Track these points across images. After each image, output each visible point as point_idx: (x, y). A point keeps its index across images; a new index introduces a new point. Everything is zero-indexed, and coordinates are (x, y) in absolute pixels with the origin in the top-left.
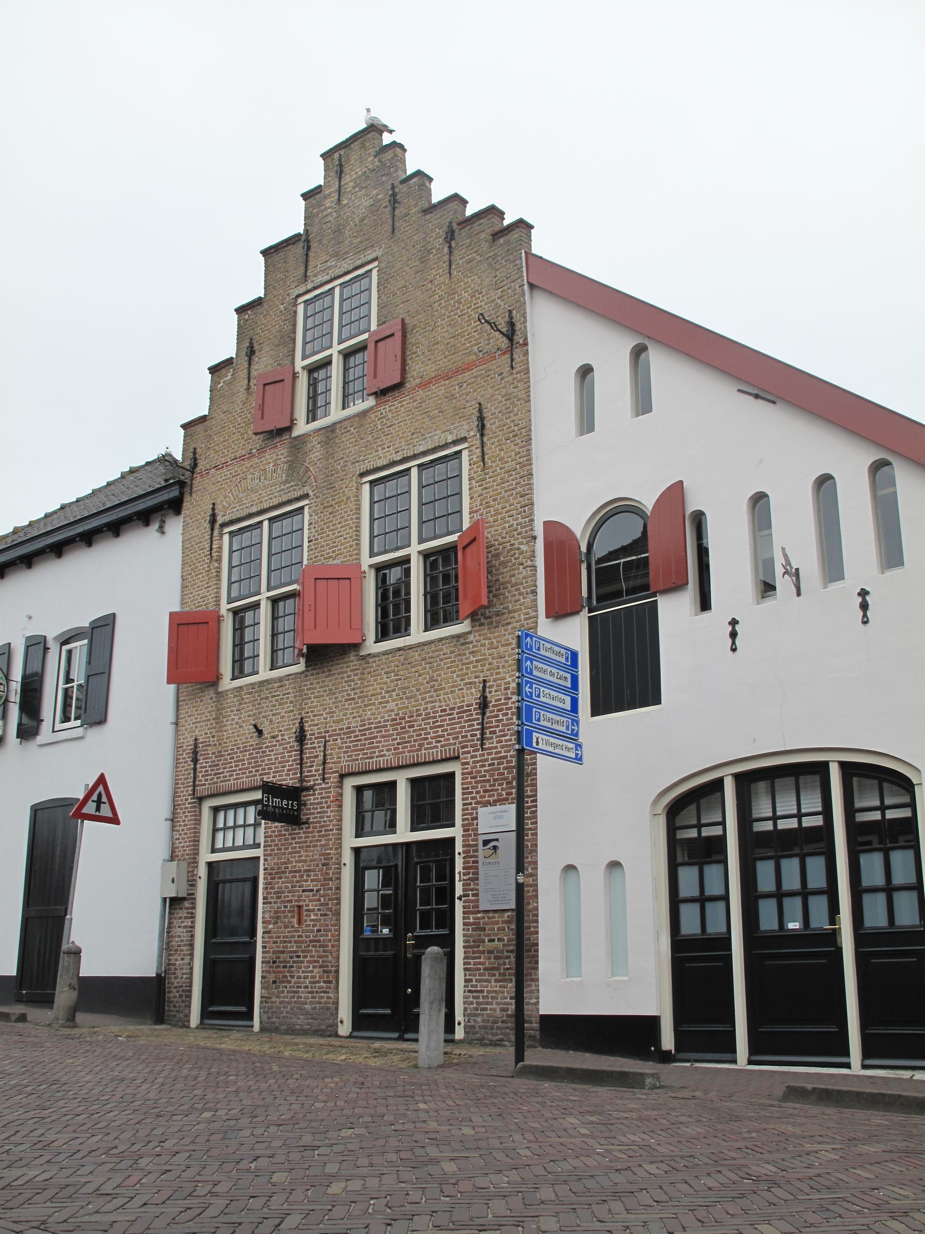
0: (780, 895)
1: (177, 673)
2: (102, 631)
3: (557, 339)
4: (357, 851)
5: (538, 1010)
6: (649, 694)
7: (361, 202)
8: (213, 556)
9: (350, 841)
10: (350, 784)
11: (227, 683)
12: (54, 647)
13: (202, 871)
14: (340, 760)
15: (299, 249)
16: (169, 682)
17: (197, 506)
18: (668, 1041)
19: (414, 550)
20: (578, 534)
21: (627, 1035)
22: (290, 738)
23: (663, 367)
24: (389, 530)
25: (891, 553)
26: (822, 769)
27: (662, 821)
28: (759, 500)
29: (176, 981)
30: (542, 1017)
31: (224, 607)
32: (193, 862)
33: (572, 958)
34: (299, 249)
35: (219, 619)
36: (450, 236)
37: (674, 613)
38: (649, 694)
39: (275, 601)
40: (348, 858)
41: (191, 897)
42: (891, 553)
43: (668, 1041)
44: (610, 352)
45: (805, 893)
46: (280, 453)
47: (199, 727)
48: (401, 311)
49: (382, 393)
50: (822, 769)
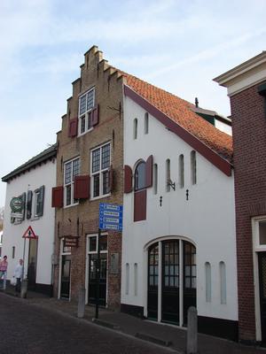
0: (169, 276)
1: (54, 205)
2: (41, 191)
3: (132, 111)
4: (90, 255)
5: (196, 312)
6: (144, 218)
7: (93, 68)
8: (62, 169)
9: (88, 252)
10: (89, 236)
11: (65, 207)
12: (34, 194)
13: (61, 258)
14: (86, 230)
15: (79, 83)
16: (53, 206)
17: (59, 156)
18: (146, 314)
19: (101, 171)
20: (132, 167)
21: (136, 310)
22: (76, 222)
23: (153, 121)
24: (96, 167)
25: (194, 180)
26: (178, 241)
27: (147, 252)
28: (168, 161)
29: (56, 286)
30: (200, 318)
31: (92, 174)
32: (59, 255)
33: (208, 298)
34: (79, 83)
35: (90, 178)
36: (109, 79)
37: (150, 192)
38: (144, 218)
39: (104, 173)
40: (87, 257)
41: (58, 264)
42: (194, 180)
43: (146, 314)
44: (140, 113)
45: (169, 276)
46: (74, 143)
47: (60, 219)
48: (99, 101)
49: (94, 126)
50: (178, 241)
